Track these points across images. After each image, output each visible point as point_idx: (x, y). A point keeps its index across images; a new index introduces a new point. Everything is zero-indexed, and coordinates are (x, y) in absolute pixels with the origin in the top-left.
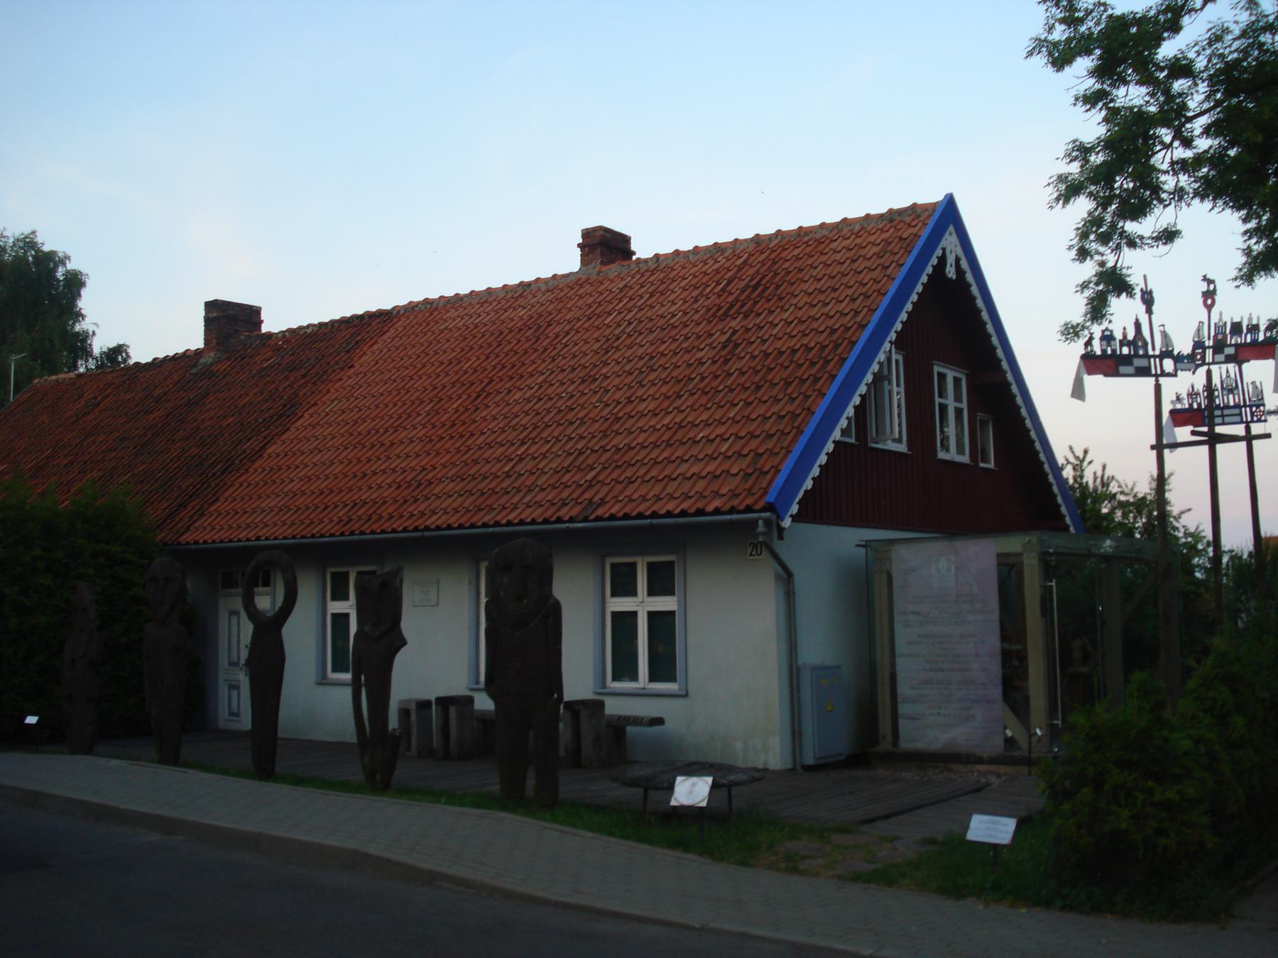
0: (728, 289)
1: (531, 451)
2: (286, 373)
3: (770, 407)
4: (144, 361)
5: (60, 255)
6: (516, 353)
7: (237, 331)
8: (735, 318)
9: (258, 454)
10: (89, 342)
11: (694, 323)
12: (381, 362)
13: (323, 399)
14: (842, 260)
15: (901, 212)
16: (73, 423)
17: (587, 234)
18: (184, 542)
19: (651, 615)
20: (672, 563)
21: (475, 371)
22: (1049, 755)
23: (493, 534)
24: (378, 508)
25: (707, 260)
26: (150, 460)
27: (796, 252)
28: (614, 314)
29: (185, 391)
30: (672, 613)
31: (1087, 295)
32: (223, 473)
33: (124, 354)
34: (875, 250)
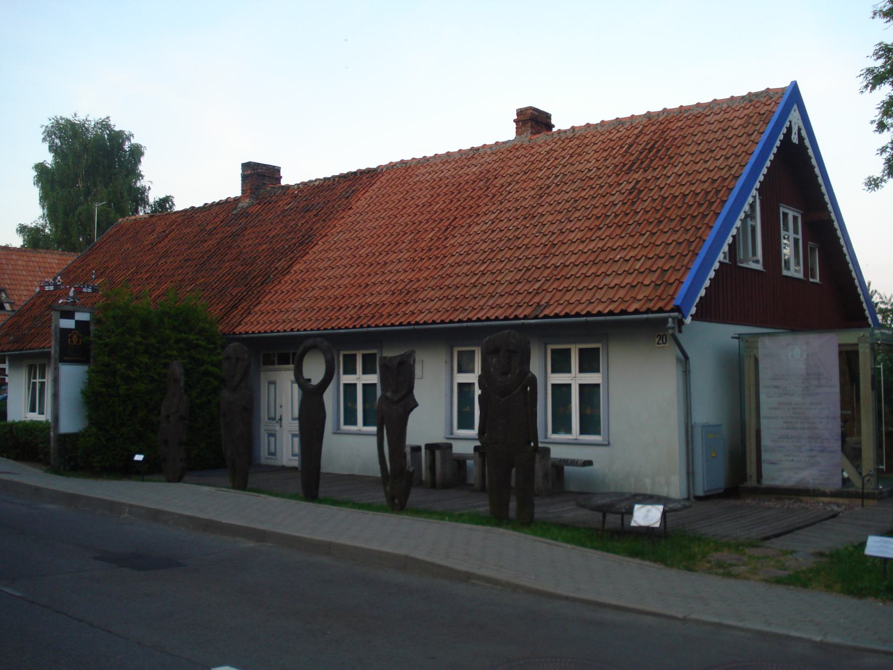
0: (630, 151)
1: (490, 268)
2: (302, 214)
3: (670, 236)
4: (197, 206)
5: (126, 133)
6: (473, 198)
7: (265, 184)
8: (637, 172)
9: (287, 270)
10: (146, 194)
11: (605, 176)
12: (372, 205)
13: (332, 232)
14: (715, 130)
15: (757, 95)
16: (149, 250)
17: (520, 112)
18: (238, 333)
19: (582, 387)
20: (598, 349)
21: (443, 211)
22: (877, 491)
23: (467, 327)
24: (380, 308)
25: (612, 130)
26: (208, 275)
27: (679, 124)
28: (544, 170)
29: (229, 226)
30: (598, 385)
31: (885, 157)
32: (262, 284)
33: (170, 203)
34: (740, 122)
